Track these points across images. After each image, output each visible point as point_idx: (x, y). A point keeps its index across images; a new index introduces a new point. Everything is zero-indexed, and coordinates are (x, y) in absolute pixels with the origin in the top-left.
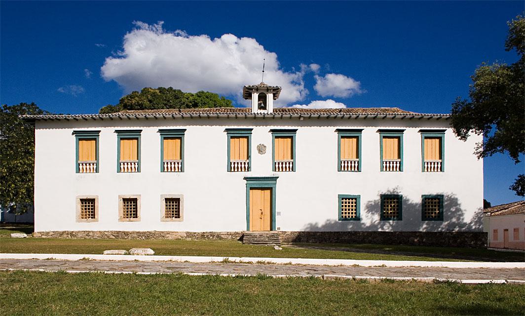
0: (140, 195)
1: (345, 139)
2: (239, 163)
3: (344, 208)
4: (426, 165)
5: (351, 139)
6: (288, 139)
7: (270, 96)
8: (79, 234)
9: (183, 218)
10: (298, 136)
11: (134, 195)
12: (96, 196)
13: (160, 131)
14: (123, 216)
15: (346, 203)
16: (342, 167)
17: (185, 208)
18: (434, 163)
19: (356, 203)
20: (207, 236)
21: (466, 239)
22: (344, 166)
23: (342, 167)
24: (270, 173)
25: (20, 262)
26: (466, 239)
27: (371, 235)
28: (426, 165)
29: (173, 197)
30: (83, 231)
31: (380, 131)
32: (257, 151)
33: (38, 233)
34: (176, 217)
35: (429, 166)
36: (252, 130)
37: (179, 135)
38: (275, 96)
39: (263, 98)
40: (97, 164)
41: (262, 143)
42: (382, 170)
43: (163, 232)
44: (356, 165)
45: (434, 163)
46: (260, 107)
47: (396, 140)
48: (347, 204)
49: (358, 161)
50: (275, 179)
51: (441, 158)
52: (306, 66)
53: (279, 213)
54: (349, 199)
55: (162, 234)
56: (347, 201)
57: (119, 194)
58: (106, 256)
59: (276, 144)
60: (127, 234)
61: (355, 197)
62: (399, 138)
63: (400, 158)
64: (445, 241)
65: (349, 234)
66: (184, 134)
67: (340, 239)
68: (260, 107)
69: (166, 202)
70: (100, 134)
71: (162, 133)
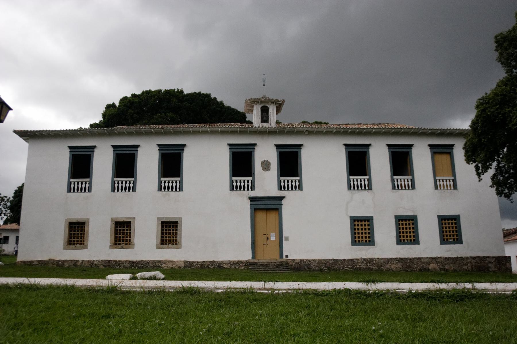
0: (134, 218)
3: (357, 231)
7: (272, 110)
8: (65, 264)
11: (127, 218)
15: (358, 225)
20: (208, 265)
21: (490, 265)
24: (275, 192)
26: (490, 265)
27: (388, 262)
29: (171, 220)
38: (278, 110)
39: (265, 111)
40: (454, 181)
48: (360, 227)
49: (251, 181)
50: (281, 198)
53: (287, 239)
54: (365, 221)
56: (360, 223)
61: (412, 218)
64: (467, 268)
65: (365, 262)
67: (355, 267)
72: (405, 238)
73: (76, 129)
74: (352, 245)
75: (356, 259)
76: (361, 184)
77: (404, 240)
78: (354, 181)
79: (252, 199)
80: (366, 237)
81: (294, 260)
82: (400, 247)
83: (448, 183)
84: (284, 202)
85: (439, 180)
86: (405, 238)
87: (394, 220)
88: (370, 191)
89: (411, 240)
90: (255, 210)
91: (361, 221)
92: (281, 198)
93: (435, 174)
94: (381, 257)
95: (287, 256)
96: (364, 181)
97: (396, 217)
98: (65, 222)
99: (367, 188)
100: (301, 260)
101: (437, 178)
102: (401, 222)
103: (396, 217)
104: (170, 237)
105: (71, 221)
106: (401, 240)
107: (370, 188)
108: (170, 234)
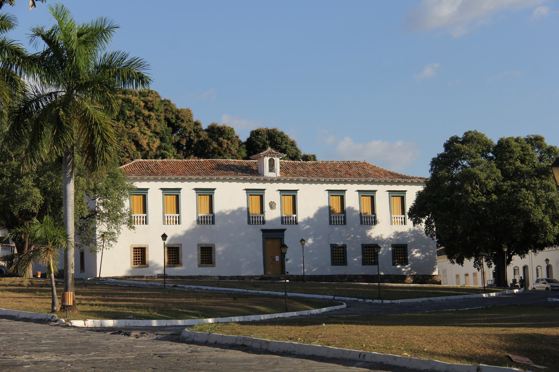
0: (181, 244)
9: (215, 264)
10: (217, 196)
15: (367, 250)
18: (258, 217)
19: (404, 250)
25: (121, 307)
41: (273, 201)
45: (258, 217)
50: (283, 231)
52: (181, 142)
58: (529, 315)
59: (392, 200)
63: (146, 213)
70: (181, 191)
71: (197, 192)
72: (337, 261)
73: (166, 182)
74: (332, 265)
75: (335, 275)
76: (207, 220)
77: (336, 262)
78: (334, 218)
79: (264, 231)
80: (341, 259)
81: (293, 275)
82: (364, 266)
83: (398, 220)
84: (285, 233)
85: (364, 217)
86: (337, 261)
87: (361, 247)
88: (345, 225)
89: (341, 262)
90: (265, 239)
91: (399, 248)
92: (284, 230)
93: (391, 213)
94: (351, 274)
95: (288, 273)
96: (341, 218)
97: (362, 245)
98: (131, 247)
99: (343, 224)
100: (297, 275)
101: (166, 215)
102: (365, 249)
103: (362, 245)
104: (205, 258)
105: (135, 247)
106: (365, 262)
107: (345, 223)
108: (205, 256)
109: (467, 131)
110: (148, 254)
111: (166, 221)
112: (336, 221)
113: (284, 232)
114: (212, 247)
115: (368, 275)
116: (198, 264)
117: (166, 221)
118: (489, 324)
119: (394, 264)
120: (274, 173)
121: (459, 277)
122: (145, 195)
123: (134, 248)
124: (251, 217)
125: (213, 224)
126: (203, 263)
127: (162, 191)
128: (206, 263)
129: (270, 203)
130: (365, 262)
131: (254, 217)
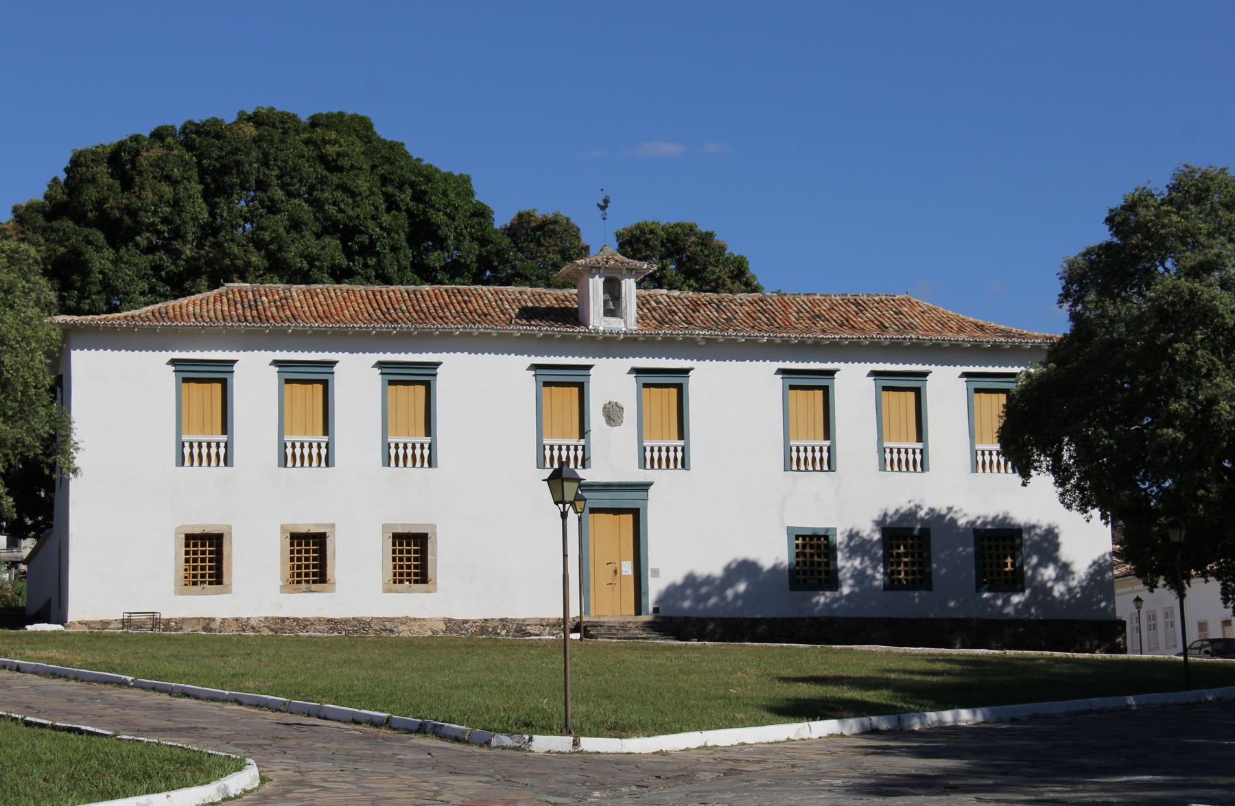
0: (333, 526)
1: (891, 392)
2: (664, 449)
4: (888, 456)
5: (903, 394)
6: (817, 391)
9: (435, 584)
10: (694, 385)
11: (318, 525)
12: (227, 526)
13: (173, 362)
14: (391, 577)
16: (793, 462)
17: (441, 558)
20: (495, 628)
22: (798, 459)
23: (793, 462)
28: (980, 458)
30: (194, 618)
31: (875, 374)
32: (603, 419)
33: (79, 623)
34: (211, 583)
35: (987, 458)
36: (332, 364)
37: (424, 377)
41: (614, 400)
42: (181, 462)
43: (391, 620)
44: (679, 455)
46: (609, 313)
47: (819, 393)
51: (681, 435)
55: (386, 626)
57: (283, 523)
60: (303, 623)
62: (680, 388)
63: (829, 439)
66: (435, 375)
68: (609, 313)
69: (187, 545)
70: (335, 369)
96: (914, 453)
99: (826, 467)
105: (190, 531)
107: (924, 467)
109: (1117, 202)
110: (230, 555)
111: (889, 461)
112: (806, 459)
113: (647, 490)
114: (427, 534)
115: (901, 619)
116: (384, 584)
117: (889, 461)
118: (363, 711)
119: (979, 588)
120: (619, 319)
121: (1206, 630)
122: (429, 382)
123: (189, 537)
124: (547, 448)
125: (830, 469)
126: (401, 582)
127: (277, 369)
128: (307, 582)
129: (605, 408)
130: (798, 580)
131: (556, 448)
